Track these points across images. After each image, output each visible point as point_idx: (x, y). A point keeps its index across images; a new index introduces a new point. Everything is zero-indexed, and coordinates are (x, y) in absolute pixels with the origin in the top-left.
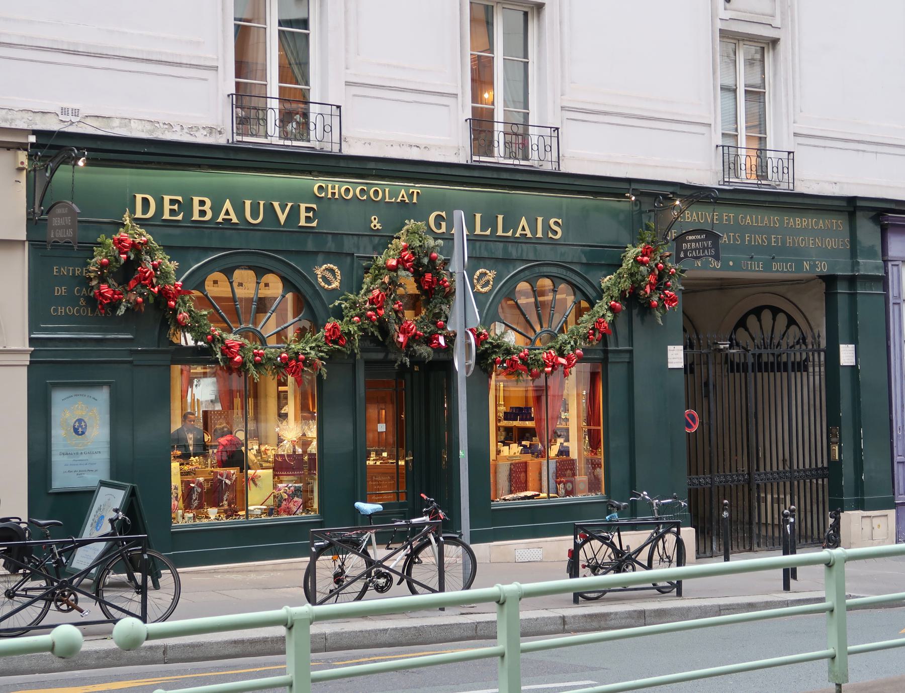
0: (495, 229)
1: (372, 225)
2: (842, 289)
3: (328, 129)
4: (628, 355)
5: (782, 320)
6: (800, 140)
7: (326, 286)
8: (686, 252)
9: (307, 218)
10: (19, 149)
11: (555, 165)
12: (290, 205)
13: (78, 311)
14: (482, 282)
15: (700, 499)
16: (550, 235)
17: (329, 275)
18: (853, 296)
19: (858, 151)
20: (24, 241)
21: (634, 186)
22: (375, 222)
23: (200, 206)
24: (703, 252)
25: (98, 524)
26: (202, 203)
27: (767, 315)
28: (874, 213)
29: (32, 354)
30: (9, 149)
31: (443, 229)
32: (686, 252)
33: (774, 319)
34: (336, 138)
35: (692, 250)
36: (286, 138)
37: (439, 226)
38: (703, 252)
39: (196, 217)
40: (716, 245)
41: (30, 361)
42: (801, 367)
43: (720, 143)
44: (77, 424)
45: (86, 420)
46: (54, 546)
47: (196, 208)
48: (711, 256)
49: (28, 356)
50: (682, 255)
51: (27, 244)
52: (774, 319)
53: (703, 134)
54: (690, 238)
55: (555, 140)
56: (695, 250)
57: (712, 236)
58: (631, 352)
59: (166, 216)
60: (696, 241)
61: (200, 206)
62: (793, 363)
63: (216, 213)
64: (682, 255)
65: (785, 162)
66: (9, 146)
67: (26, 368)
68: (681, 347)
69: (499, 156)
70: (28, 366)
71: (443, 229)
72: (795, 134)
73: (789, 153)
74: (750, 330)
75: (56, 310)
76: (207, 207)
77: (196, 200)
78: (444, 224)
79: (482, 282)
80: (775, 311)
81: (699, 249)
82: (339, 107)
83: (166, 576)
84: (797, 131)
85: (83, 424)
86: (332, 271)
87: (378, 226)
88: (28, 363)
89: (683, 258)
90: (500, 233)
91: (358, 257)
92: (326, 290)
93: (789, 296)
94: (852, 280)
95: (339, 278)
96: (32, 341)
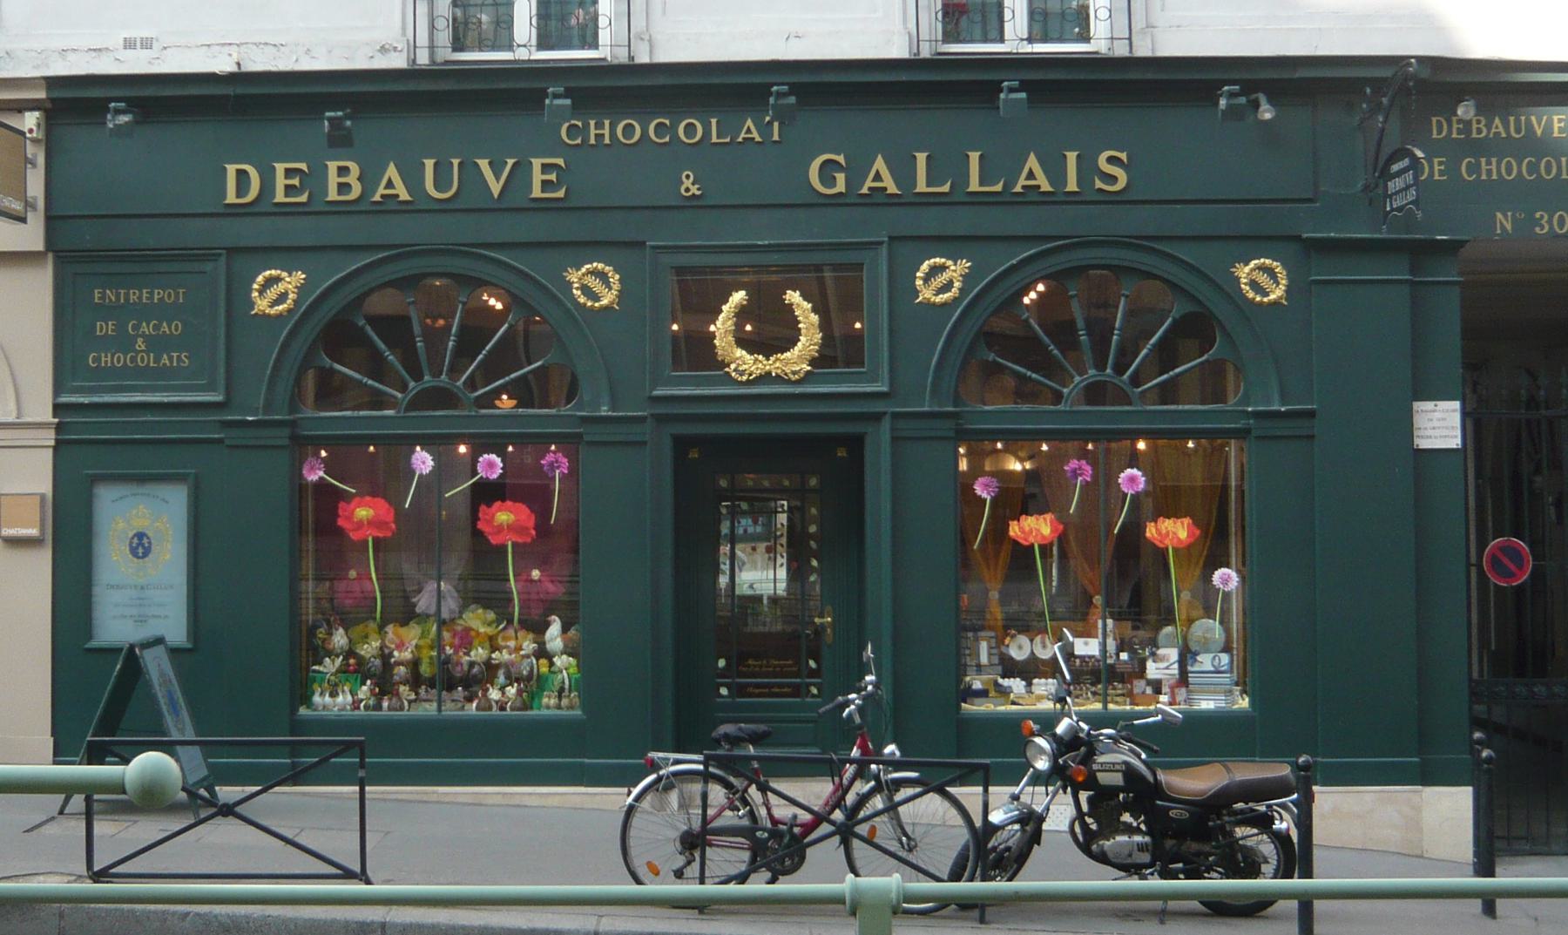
31: (841, 186)
39: (333, 195)
44: (136, 541)
45: (150, 534)
47: (333, 180)
59: (280, 197)
71: (841, 186)
76: (352, 179)
77: (333, 166)
85: (145, 541)
87: (694, 190)
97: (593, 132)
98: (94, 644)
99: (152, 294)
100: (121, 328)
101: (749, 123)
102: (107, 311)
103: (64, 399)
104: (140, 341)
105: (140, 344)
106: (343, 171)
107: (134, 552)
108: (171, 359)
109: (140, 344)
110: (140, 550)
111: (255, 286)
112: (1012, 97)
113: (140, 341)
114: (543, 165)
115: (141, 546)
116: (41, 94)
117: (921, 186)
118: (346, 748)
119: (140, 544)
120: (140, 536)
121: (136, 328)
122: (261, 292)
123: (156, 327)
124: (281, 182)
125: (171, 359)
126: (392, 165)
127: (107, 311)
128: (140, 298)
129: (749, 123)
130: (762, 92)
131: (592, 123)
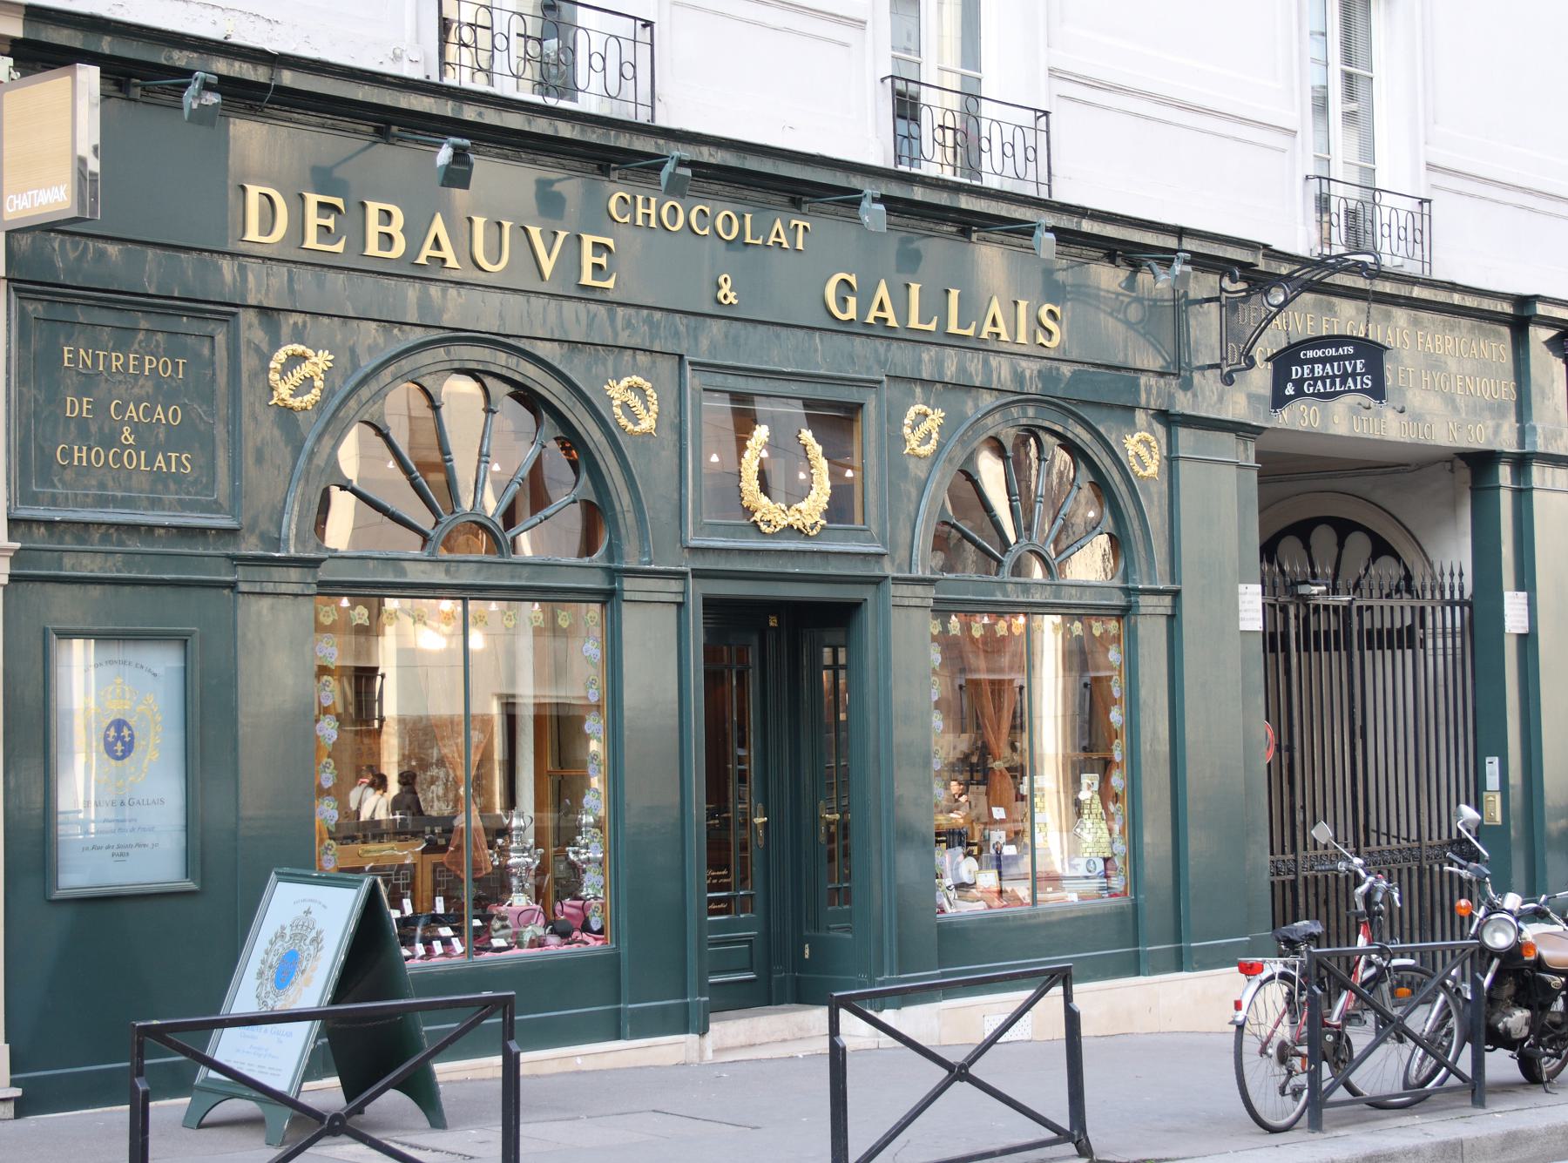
0: (944, 321)
2: (1505, 473)
4: (1167, 600)
6: (1437, 178)
7: (630, 427)
9: (597, 267)
14: (920, 433)
15: (1301, 891)
16: (1041, 339)
17: (634, 401)
18: (1523, 495)
21: (1190, 244)
22: (726, 288)
24: (1343, 383)
26: (387, 216)
27: (1323, 538)
31: (852, 313)
32: (1299, 384)
33: (1341, 545)
34: (644, 96)
35: (1315, 380)
38: (1343, 383)
39: (372, 249)
42: (1405, 638)
43: (1311, 173)
44: (112, 733)
45: (132, 722)
46: (1292, 877)
47: (374, 227)
48: (1362, 391)
50: (1290, 390)
53: (1284, 151)
54: (1310, 354)
55: (1042, 137)
56: (1323, 379)
57: (1372, 353)
58: (1176, 594)
59: (311, 241)
61: (380, 223)
64: (1290, 390)
65: (1418, 217)
68: (1259, 587)
69: (936, 163)
71: (852, 313)
72: (1431, 167)
73: (1422, 201)
74: (1345, 552)
76: (395, 228)
77: (373, 208)
78: (852, 301)
79: (920, 433)
80: (1344, 528)
81: (1333, 378)
82: (648, 24)
83: (466, 1075)
84: (1433, 161)
85: (126, 732)
86: (640, 391)
87: (732, 298)
89: (1291, 398)
91: (691, 363)
92: (632, 433)
93: (1377, 496)
94: (1521, 463)
95: (654, 408)
97: (640, 210)
98: (58, 895)
99: (141, 361)
100: (100, 408)
101: (778, 225)
102: (88, 381)
103: (25, 513)
104: (126, 430)
105: (127, 436)
106: (387, 216)
107: (109, 748)
108: (168, 461)
109: (127, 436)
110: (119, 747)
111: (906, 421)
112: (873, 214)
113: (126, 430)
114: (321, 205)
115: (119, 741)
116: (1507, 308)
117: (914, 323)
118: (490, 1006)
119: (119, 738)
120: (119, 724)
121: (121, 409)
122: (913, 429)
123: (149, 412)
124: (313, 219)
125: (168, 461)
126: (438, 217)
127: (88, 381)
128: (126, 365)
129: (778, 225)
130: (850, 200)
131: (640, 198)
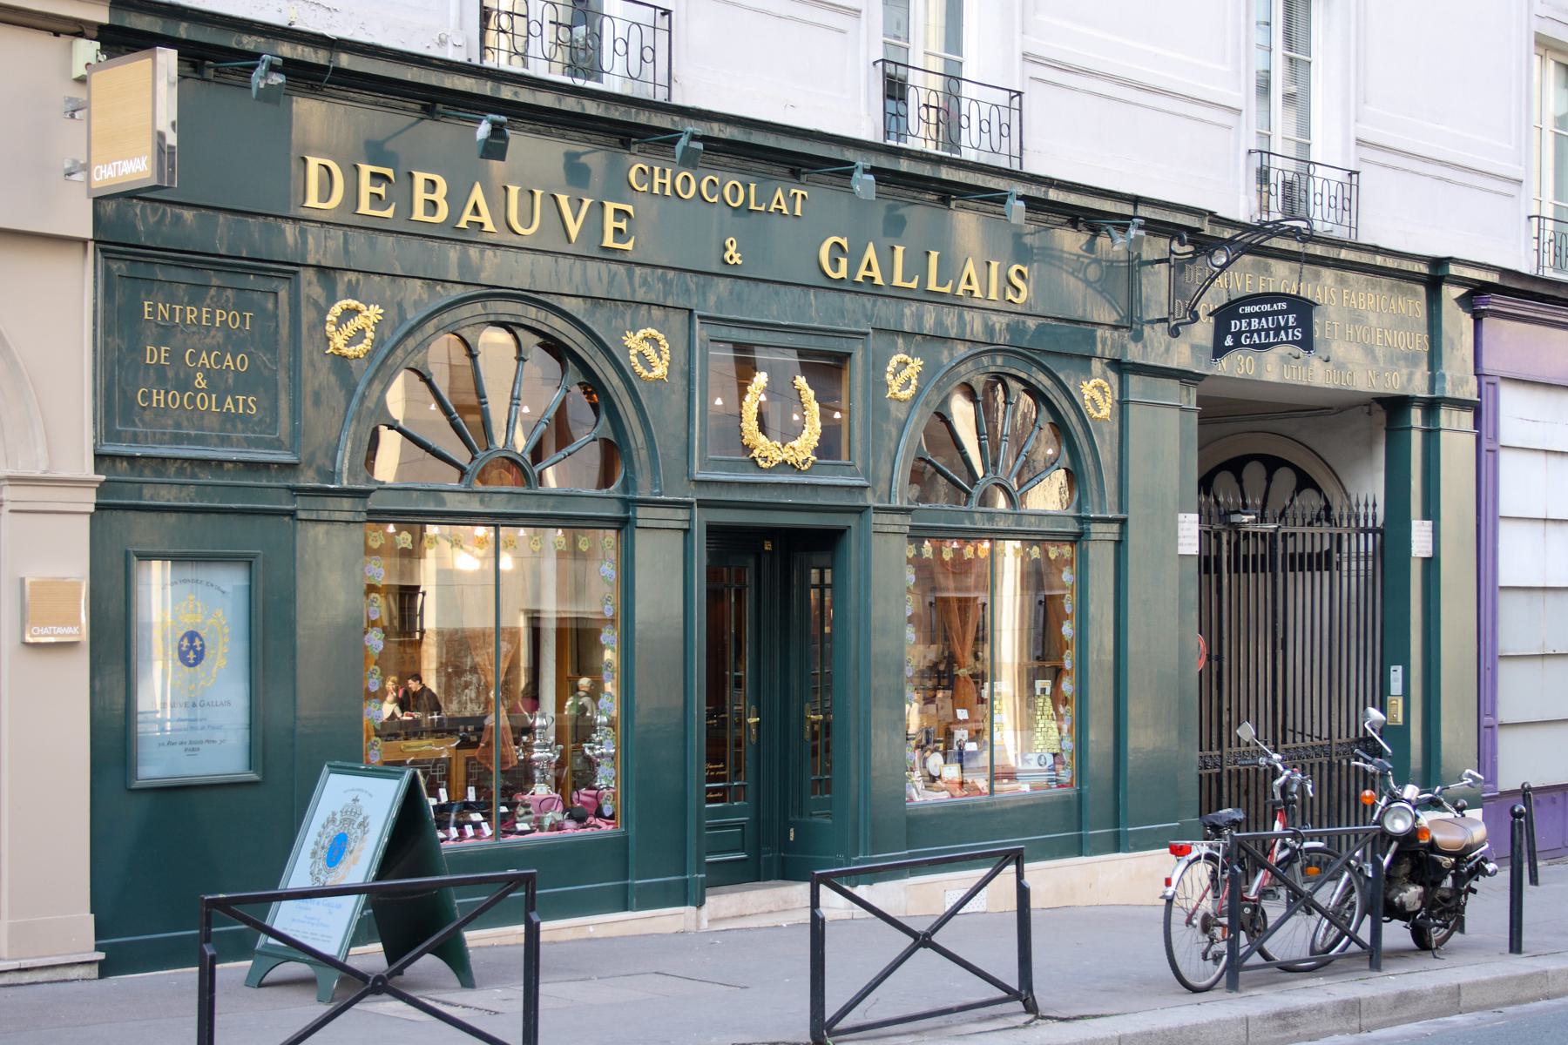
0: (924, 280)
1: (727, 256)
3: (648, 55)
4: (1115, 527)
5: (1285, 478)
7: (645, 373)
8: (1237, 336)
10: (80, 35)
11: (1016, 162)
12: (587, 202)
13: (192, 400)
16: (1010, 296)
17: (649, 350)
19: (1440, 179)
20: (85, 242)
21: (1144, 211)
22: (732, 250)
23: (426, 191)
24: (1277, 335)
25: (336, 851)
28: (1463, 291)
29: (102, 489)
30: (57, 34)
31: (843, 272)
32: (1237, 336)
35: (1252, 332)
36: (574, 75)
37: (835, 263)
39: (419, 214)
40: (1306, 323)
41: (98, 507)
42: (1323, 561)
43: (1253, 147)
44: (186, 643)
45: (203, 633)
47: (420, 195)
49: (93, 492)
50: (1229, 342)
51: (91, 245)
52: (1269, 479)
54: (1248, 309)
56: (1258, 331)
58: (1123, 522)
60: (1259, 315)
61: (426, 191)
62: (1310, 555)
63: (455, 214)
64: (1229, 342)
65: (1347, 187)
66: (57, 26)
67: (87, 518)
68: (1196, 516)
70: (92, 514)
71: (843, 272)
73: (1351, 173)
75: (147, 397)
76: (439, 196)
77: (420, 178)
78: (843, 262)
81: (1267, 331)
82: (666, 12)
85: (197, 642)
86: (654, 341)
87: (736, 260)
88: (92, 509)
89: (1230, 348)
90: (932, 286)
93: (1302, 437)
95: (667, 357)
96: (99, 457)
